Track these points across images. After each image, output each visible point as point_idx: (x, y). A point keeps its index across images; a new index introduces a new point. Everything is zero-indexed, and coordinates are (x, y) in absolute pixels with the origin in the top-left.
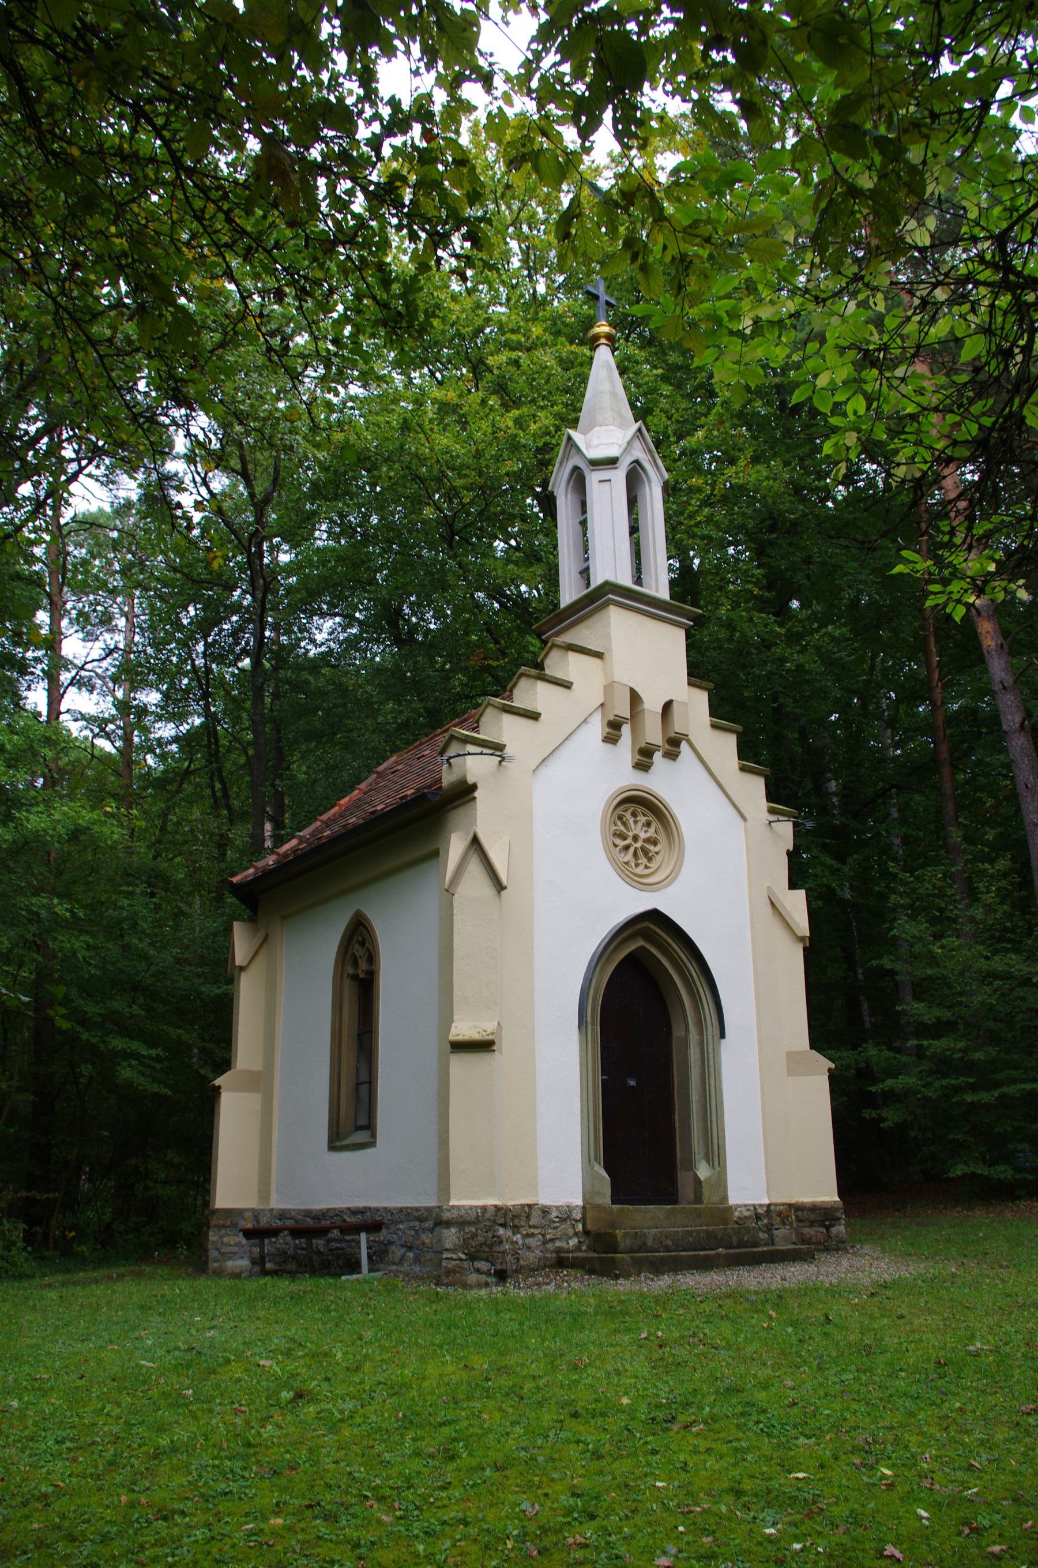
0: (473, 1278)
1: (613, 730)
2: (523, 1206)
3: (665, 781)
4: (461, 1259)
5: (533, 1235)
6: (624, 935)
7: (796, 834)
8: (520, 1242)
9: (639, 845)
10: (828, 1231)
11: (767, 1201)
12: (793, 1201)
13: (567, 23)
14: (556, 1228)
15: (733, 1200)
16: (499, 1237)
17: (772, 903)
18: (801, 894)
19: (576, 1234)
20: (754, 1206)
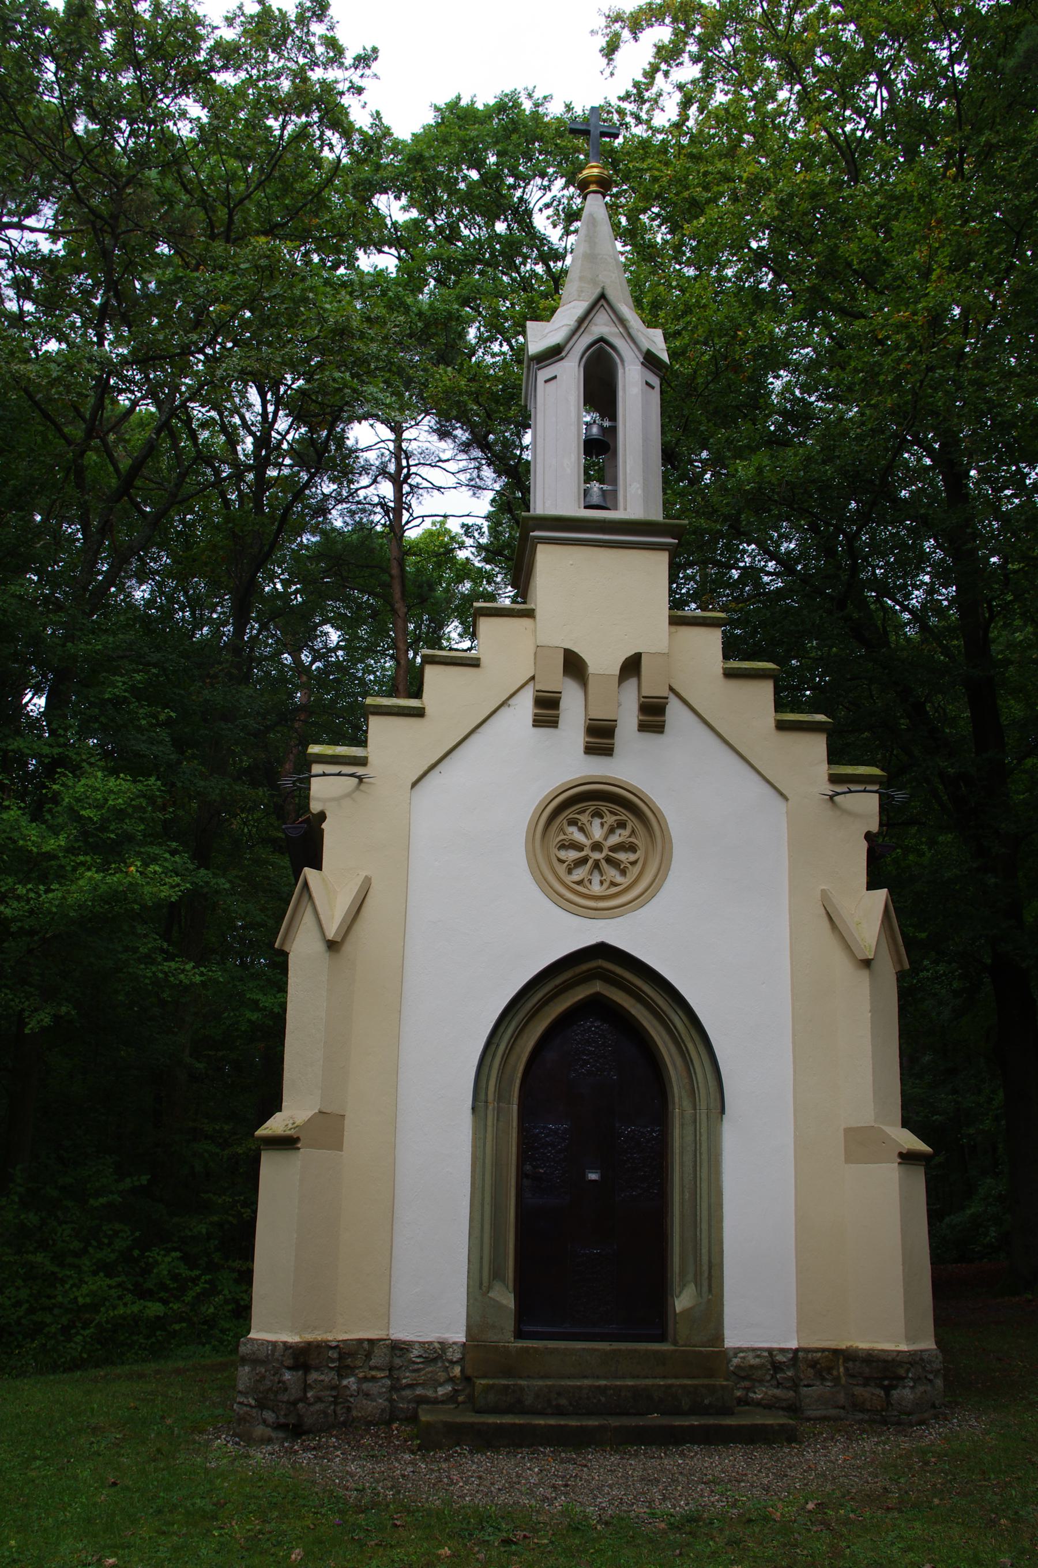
0: (260, 1430)
1: (547, 710)
2: (360, 1341)
3: (632, 765)
4: (250, 1406)
5: (374, 1379)
6: (558, 981)
7: (884, 808)
8: (354, 1387)
9: (597, 856)
10: (888, 1394)
11: (793, 1344)
12: (843, 1346)
13: (904, 2)
14: (417, 1370)
15: (732, 1340)
16: (284, 1382)
17: (828, 913)
18: (881, 895)
19: (451, 1380)
20: (770, 1351)
